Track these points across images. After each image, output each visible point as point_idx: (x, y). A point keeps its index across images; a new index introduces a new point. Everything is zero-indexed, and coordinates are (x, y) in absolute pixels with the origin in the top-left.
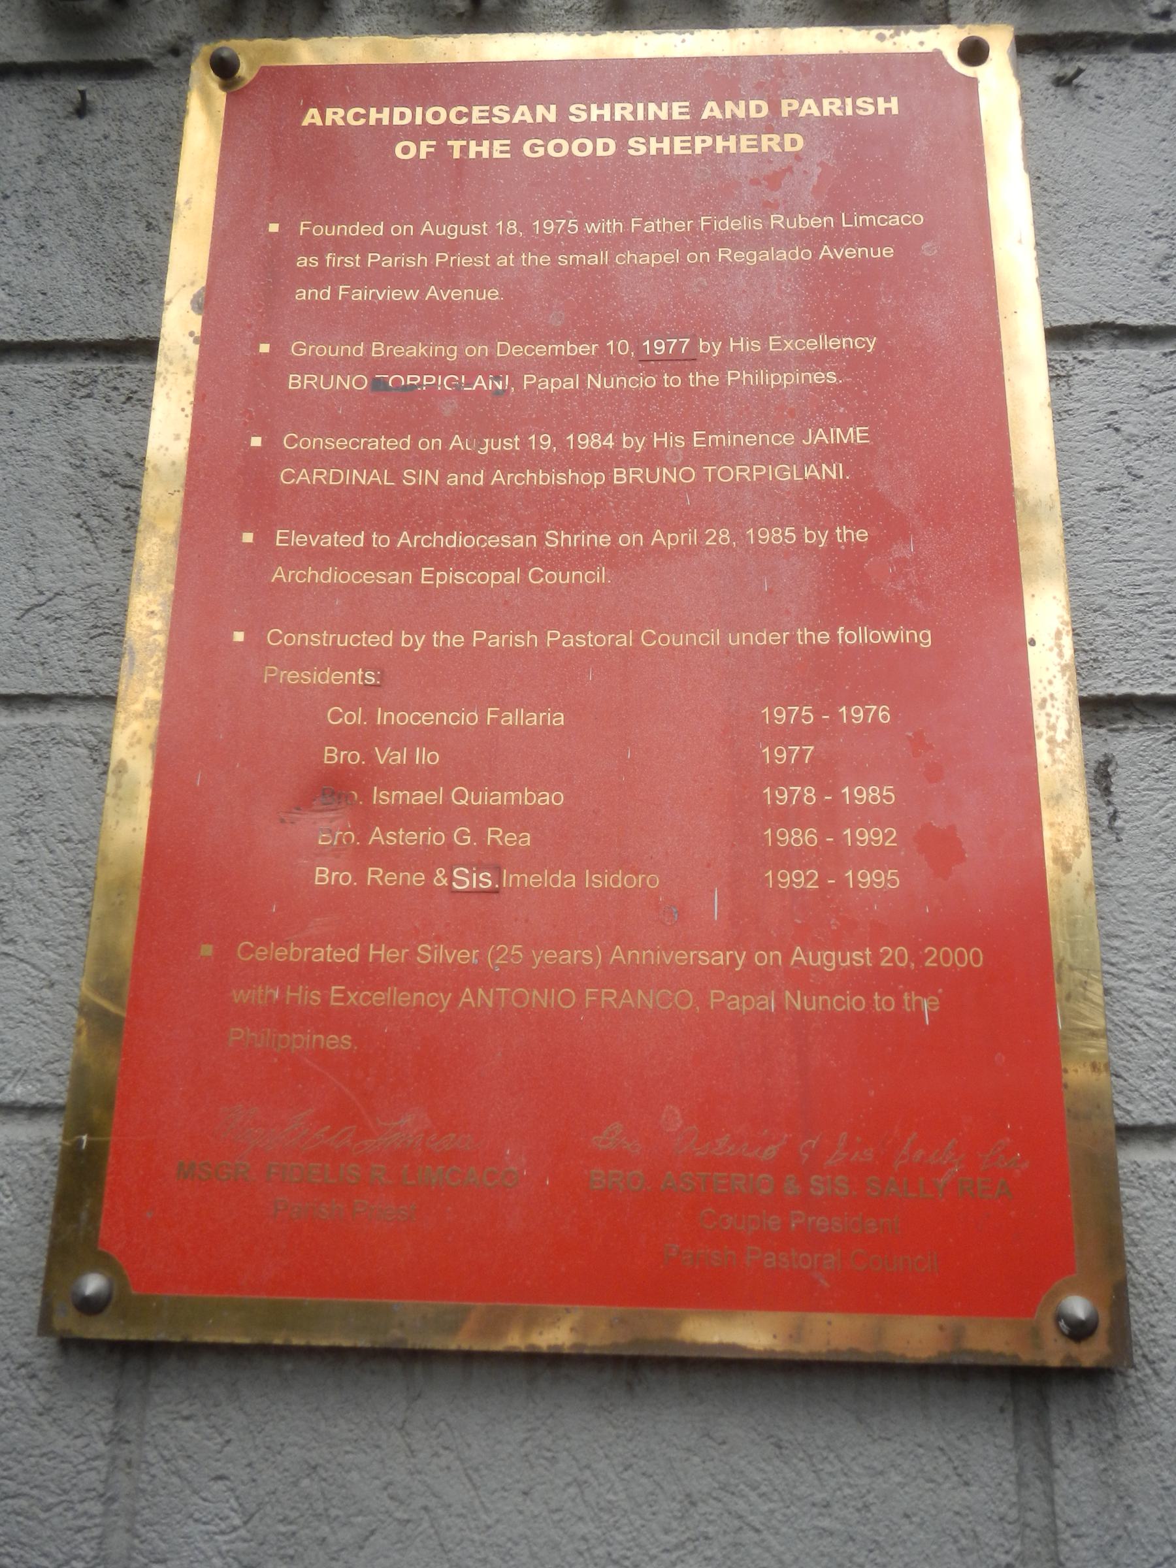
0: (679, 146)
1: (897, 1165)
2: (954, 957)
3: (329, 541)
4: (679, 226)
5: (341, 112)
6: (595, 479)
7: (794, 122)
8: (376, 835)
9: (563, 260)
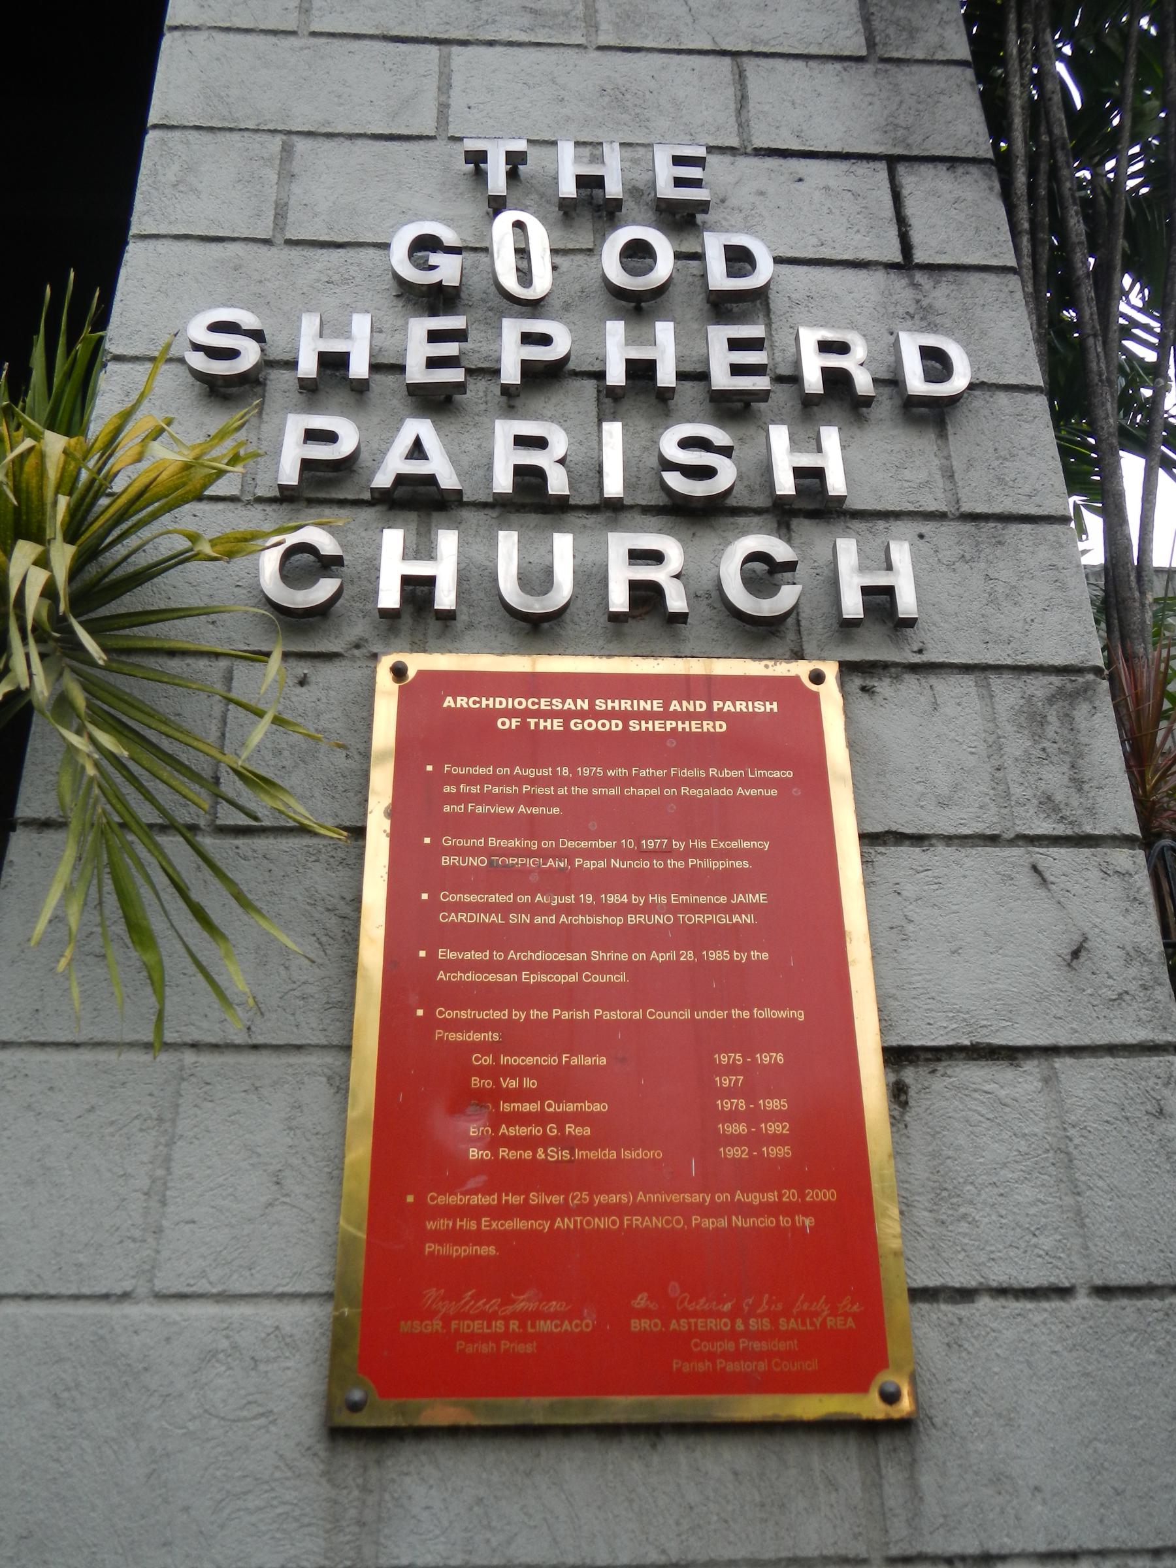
0: (658, 726)
1: (795, 1311)
2: (821, 1195)
3: (469, 955)
4: (660, 773)
5: (465, 699)
6: (618, 921)
7: (721, 715)
8: (503, 1129)
9: (595, 792)
